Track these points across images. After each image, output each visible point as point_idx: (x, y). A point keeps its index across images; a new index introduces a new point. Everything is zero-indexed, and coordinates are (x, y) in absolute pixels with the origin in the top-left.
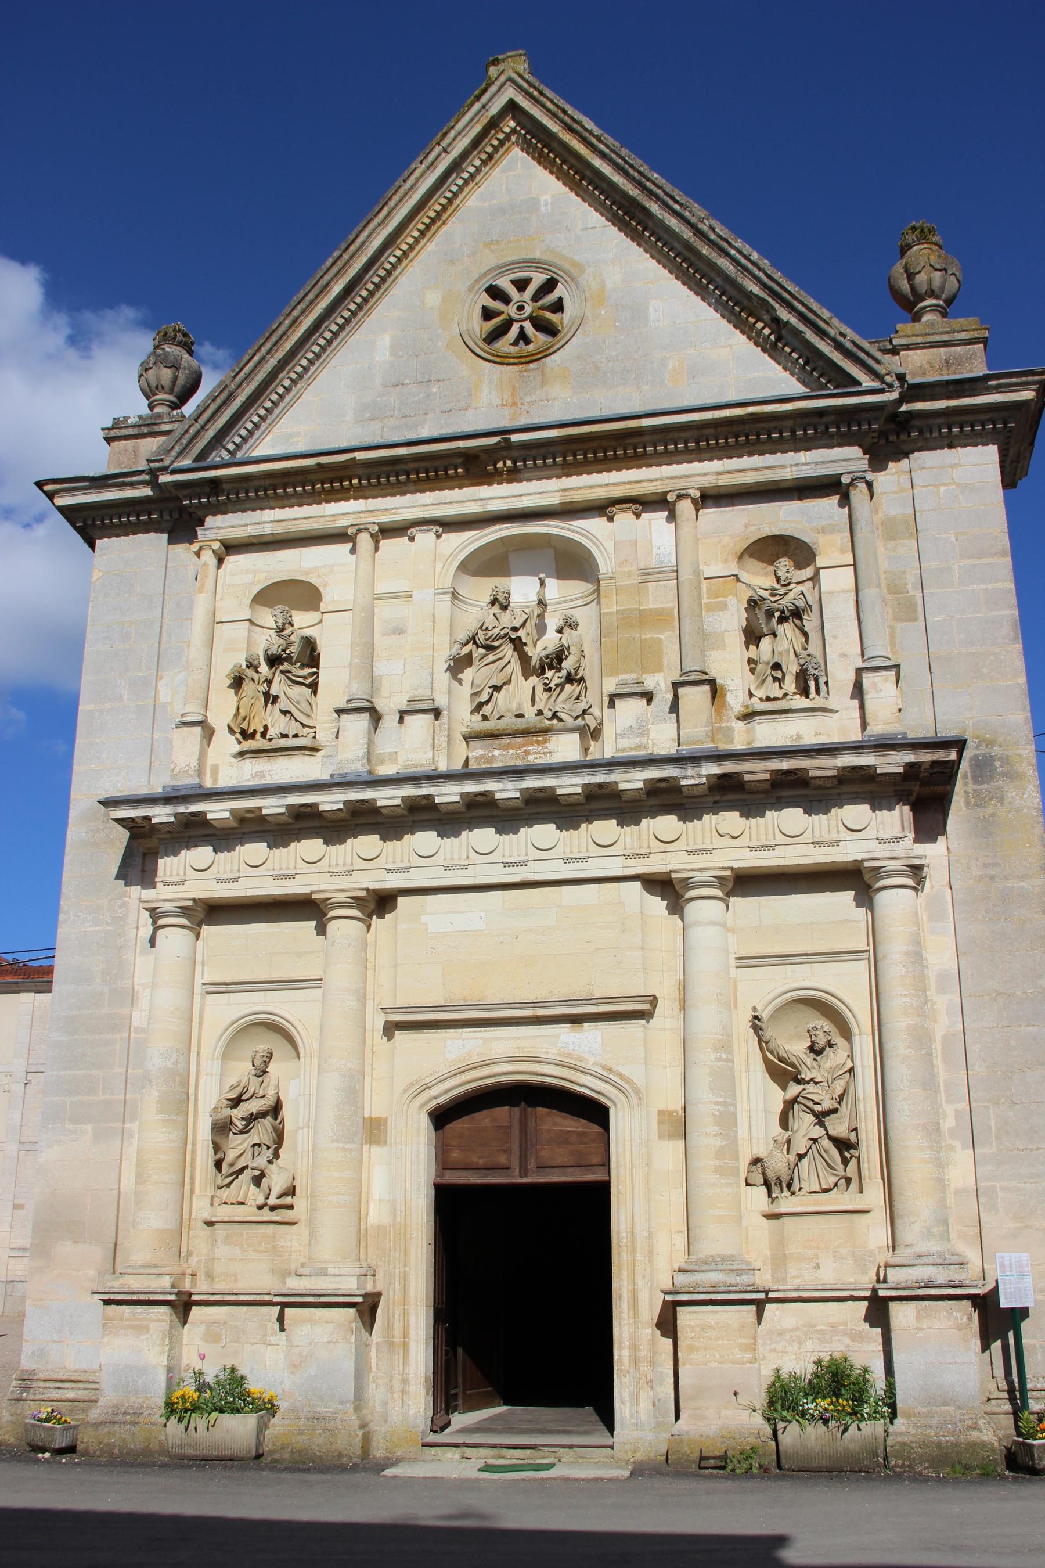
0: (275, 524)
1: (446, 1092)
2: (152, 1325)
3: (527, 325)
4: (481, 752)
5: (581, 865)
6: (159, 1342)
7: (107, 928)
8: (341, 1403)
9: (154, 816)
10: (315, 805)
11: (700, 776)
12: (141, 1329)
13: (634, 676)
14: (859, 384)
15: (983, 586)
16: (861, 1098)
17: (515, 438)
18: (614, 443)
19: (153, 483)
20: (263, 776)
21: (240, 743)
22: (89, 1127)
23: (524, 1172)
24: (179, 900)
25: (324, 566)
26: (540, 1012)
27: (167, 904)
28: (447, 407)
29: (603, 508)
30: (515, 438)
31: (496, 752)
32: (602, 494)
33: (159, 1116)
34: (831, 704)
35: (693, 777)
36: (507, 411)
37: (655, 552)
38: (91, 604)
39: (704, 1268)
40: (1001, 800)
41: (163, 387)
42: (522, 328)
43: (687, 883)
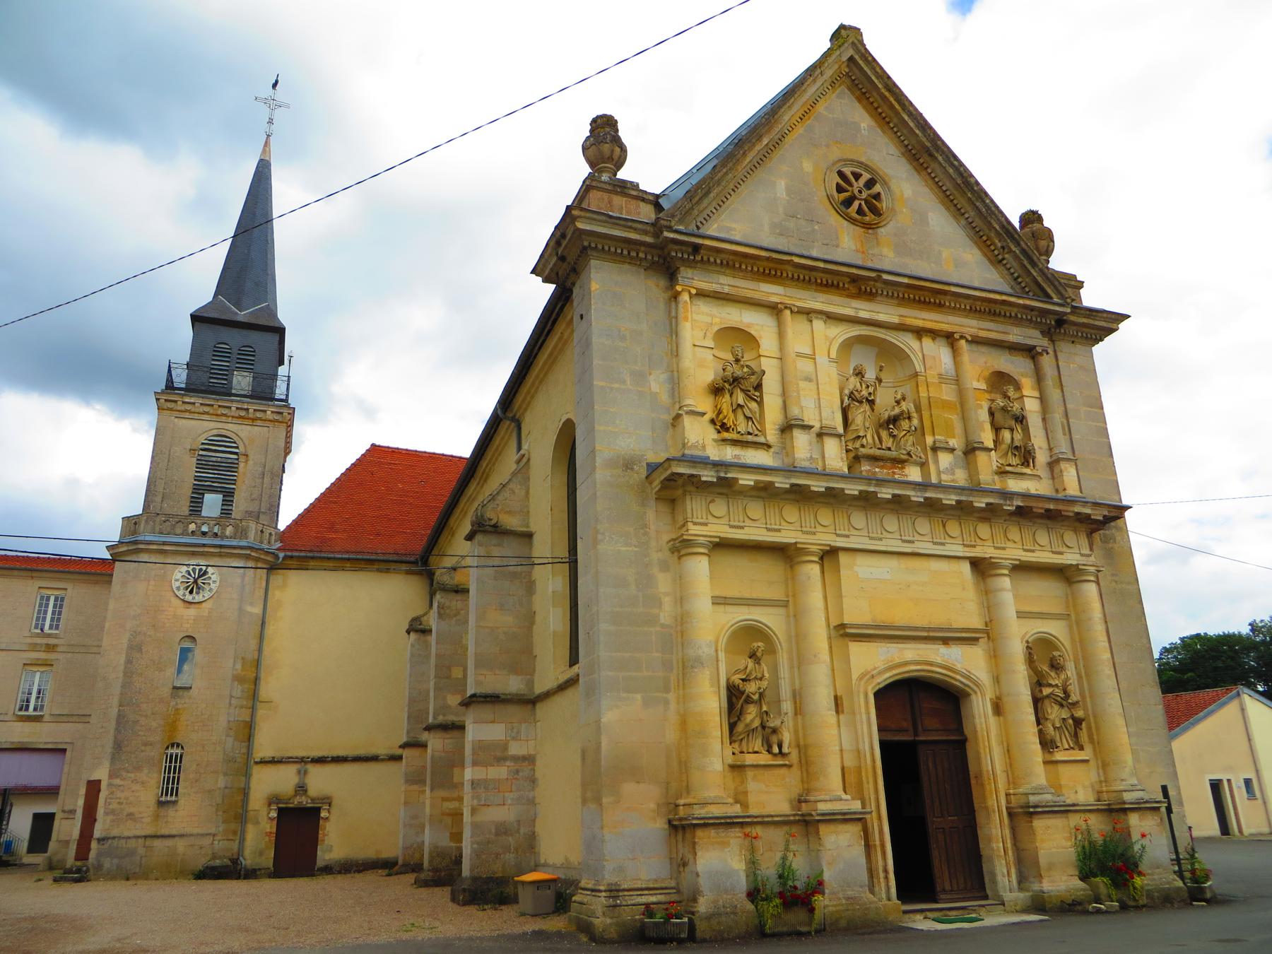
0: (730, 288)
1: (886, 680)
2: (731, 841)
3: (863, 203)
4: (868, 468)
5: (845, 539)
6: (738, 852)
7: (636, 549)
8: (861, 887)
9: (703, 475)
10: (772, 483)
11: (1013, 506)
12: (724, 844)
13: (943, 438)
14: (1051, 298)
15: (1095, 424)
16: (33, 575)
17: (885, 277)
18: (930, 294)
19: (657, 234)
20: (740, 459)
21: (719, 432)
22: (639, 696)
23: (916, 734)
24: (710, 537)
25: (757, 325)
26: (932, 634)
27: (701, 538)
28: (825, 242)
29: (919, 333)
30: (885, 277)
31: (877, 470)
32: (920, 323)
33: (712, 689)
34: (1038, 473)
35: (1009, 505)
36: (860, 255)
37: (943, 366)
38: (593, 307)
39: (1040, 791)
40: (1115, 542)
41: (613, 159)
42: (860, 204)
43: (995, 566)
